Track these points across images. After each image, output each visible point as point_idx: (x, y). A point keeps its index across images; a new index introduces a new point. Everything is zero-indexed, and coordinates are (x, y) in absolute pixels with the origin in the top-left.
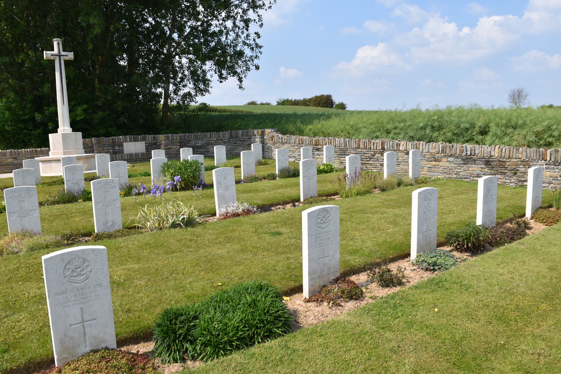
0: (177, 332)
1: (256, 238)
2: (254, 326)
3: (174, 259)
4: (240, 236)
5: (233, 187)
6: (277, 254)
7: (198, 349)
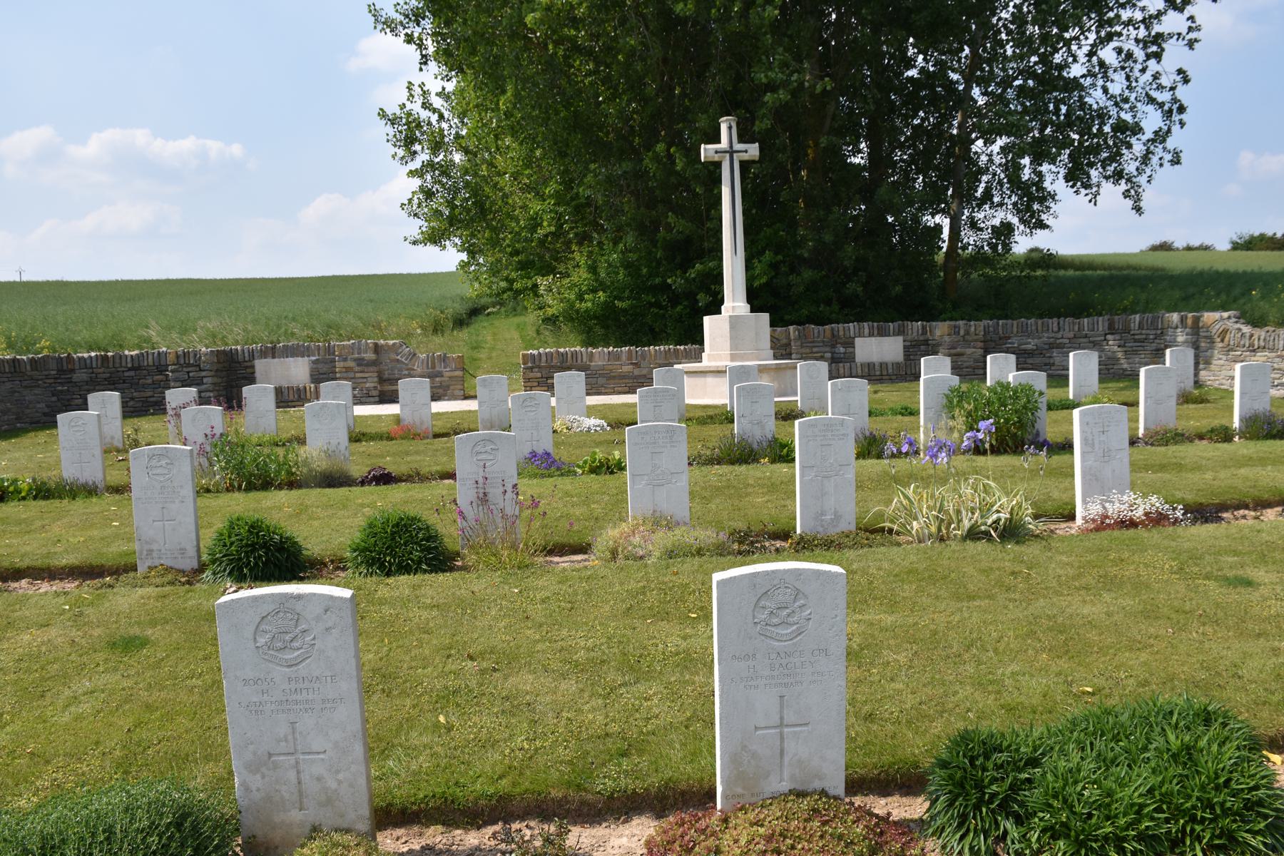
0: (988, 787)
1: (1181, 588)
2: (1184, 813)
3: (975, 614)
4: (1139, 576)
5: (1124, 454)
6: (1241, 634)
7: (1034, 840)
